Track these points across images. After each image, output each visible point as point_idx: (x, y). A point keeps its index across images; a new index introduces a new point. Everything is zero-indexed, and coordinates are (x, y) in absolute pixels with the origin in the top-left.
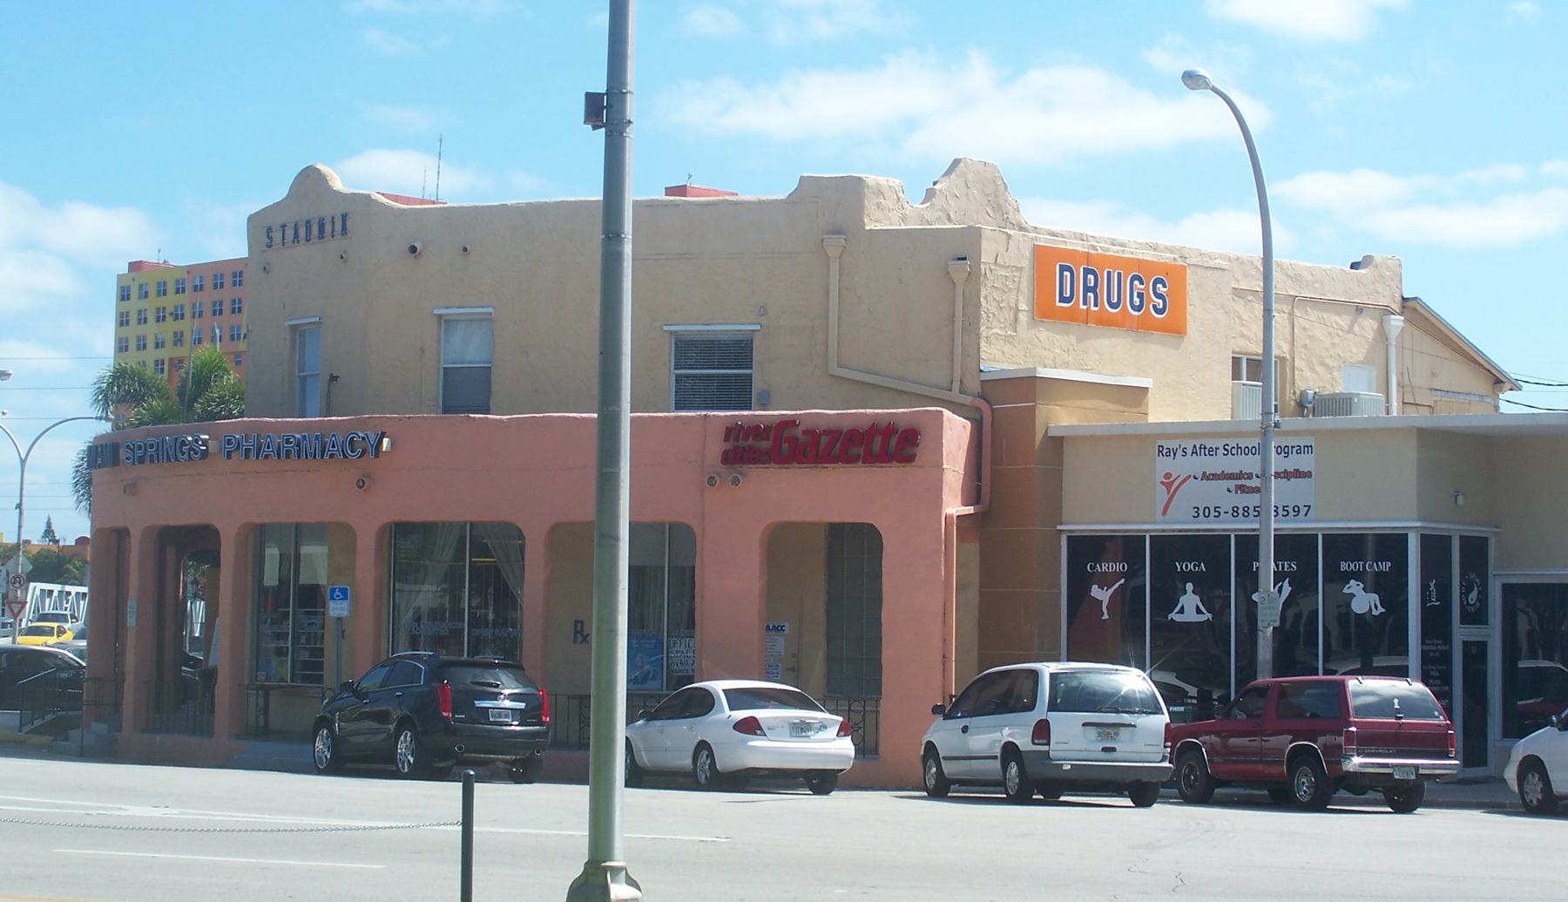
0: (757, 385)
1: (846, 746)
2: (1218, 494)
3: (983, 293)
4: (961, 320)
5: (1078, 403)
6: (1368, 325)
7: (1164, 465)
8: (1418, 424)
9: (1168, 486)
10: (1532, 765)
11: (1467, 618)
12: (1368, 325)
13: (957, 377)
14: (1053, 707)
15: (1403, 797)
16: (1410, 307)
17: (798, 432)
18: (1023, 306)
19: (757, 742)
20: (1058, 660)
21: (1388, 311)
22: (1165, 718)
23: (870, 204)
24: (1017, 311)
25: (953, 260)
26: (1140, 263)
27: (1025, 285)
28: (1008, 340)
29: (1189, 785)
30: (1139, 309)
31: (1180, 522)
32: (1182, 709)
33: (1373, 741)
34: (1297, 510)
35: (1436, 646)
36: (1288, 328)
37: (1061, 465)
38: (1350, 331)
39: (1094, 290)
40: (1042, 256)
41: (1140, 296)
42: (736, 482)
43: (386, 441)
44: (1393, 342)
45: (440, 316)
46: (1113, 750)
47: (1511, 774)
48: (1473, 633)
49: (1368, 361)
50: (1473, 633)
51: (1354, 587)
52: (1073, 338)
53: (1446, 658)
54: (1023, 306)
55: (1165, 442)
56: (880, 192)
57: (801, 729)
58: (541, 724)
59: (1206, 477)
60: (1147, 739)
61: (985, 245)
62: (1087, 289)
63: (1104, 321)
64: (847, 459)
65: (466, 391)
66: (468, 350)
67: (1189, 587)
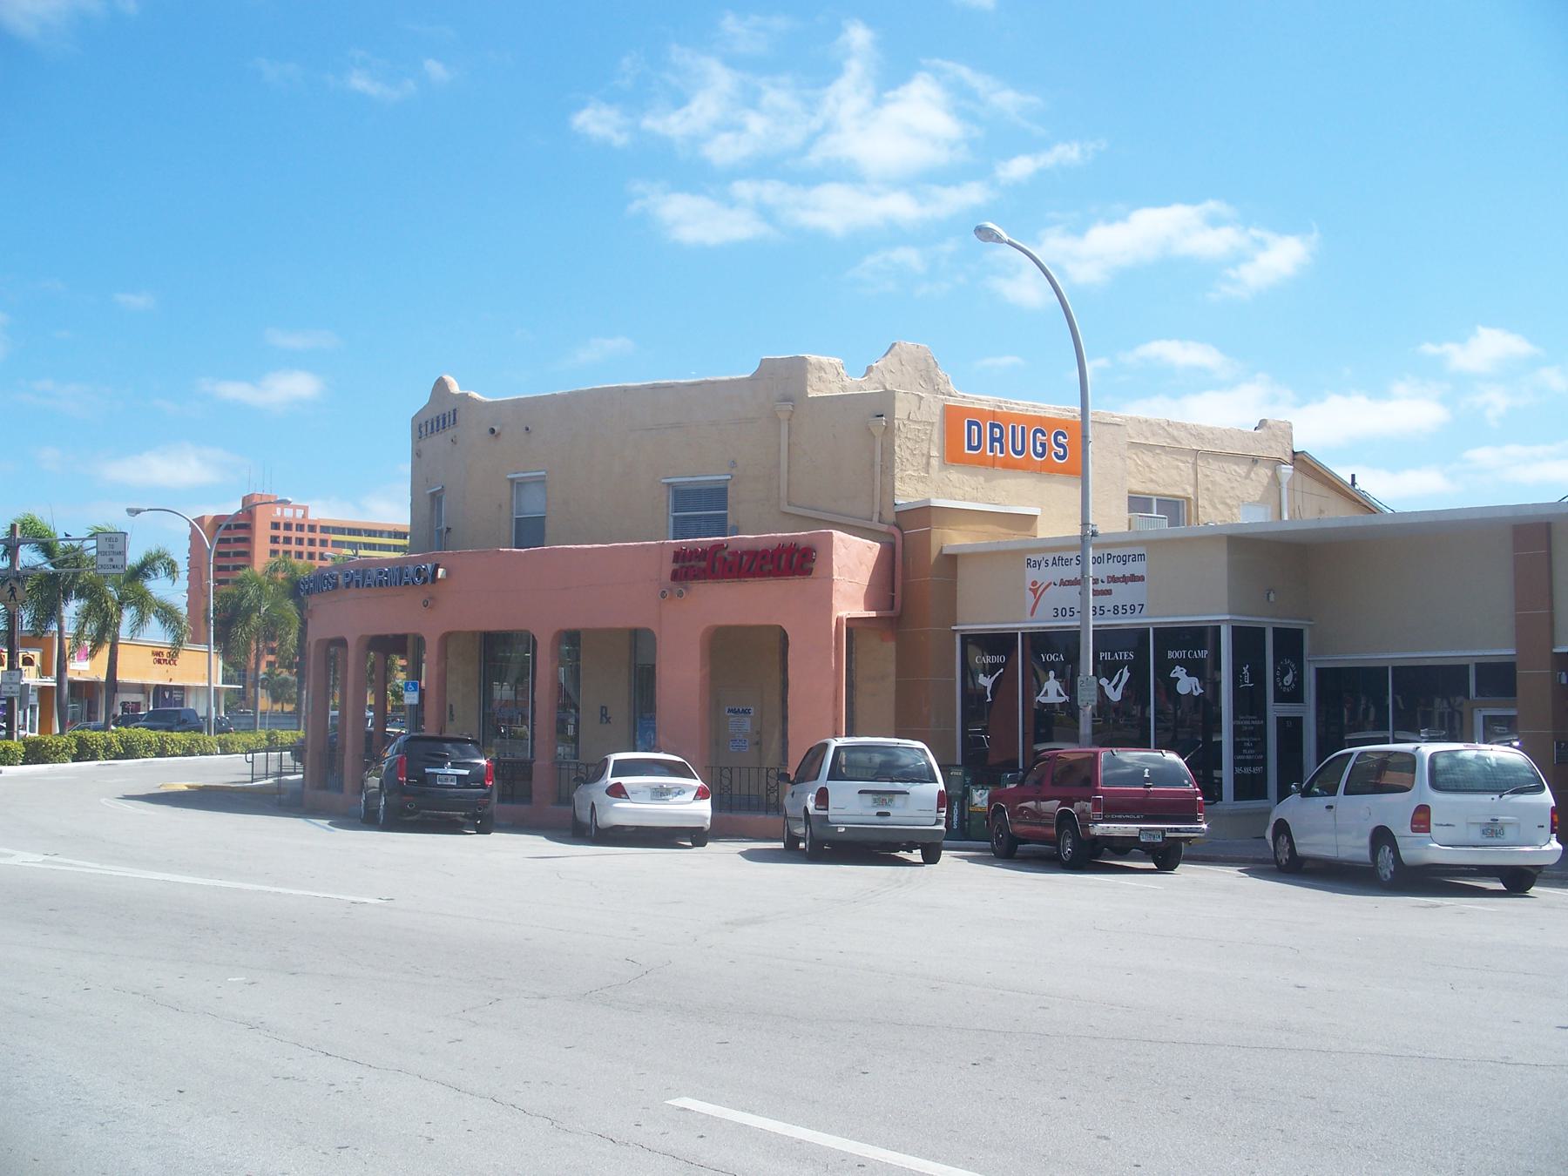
0: (730, 522)
1: (705, 808)
2: (1070, 596)
3: (897, 442)
4: (881, 465)
5: (971, 527)
6: (1263, 473)
7: (1031, 574)
8: (1229, 532)
9: (1035, 591)
10: (1282, 828)
11: (1281, 697)
12: (1263, 473)
13: (877, 509)
14: (834, 775)
15: (1166, 858)
16: (1301, 461)
17: (725, 553)
18: (934, 453)
19: (621, 804)
20: (1143, 743)
21: (1280, 462)
22: (941, 786)
23: (812, 378)
24: (929, 457)
25: (876, 413)
26: (1041, 419)
27: (936, 437)
28: (921, 480)
29: (999, 842)
30: (1042, 455)
31: (1043, 621)
32: (466, 772)
33: (1116, 809)
34: (1133, 608)
35: (1247, 722)
36: (1192, 476)
37: (955, 576)
38: (1247, 477)
39: (999, 440)
40: (952, 416)
41: (1043, 445)
42: (680, 594)
43: (440, 571)
44: (1285, 486)
45: (512, 480)
46: (887, 814)
47: (1269, 835)
48: (1288, 710)
49: (1262, 502)
50: (1288, 710)
51: (1179, 672)
52: (982, 479)
53: (1261, 731)
54: (934, 453)
55: (1030, 557)
56: (821, 368)
57: (660, 793)
58: (484, 786)
59: (1063, 583)
60: (921, 803)
61: (898, 404)
62: (993, 440)
63: (1008, 465)
64: (760, 573)
65: (529, 531)
66: (533, 505)
67: (1052, 674)
